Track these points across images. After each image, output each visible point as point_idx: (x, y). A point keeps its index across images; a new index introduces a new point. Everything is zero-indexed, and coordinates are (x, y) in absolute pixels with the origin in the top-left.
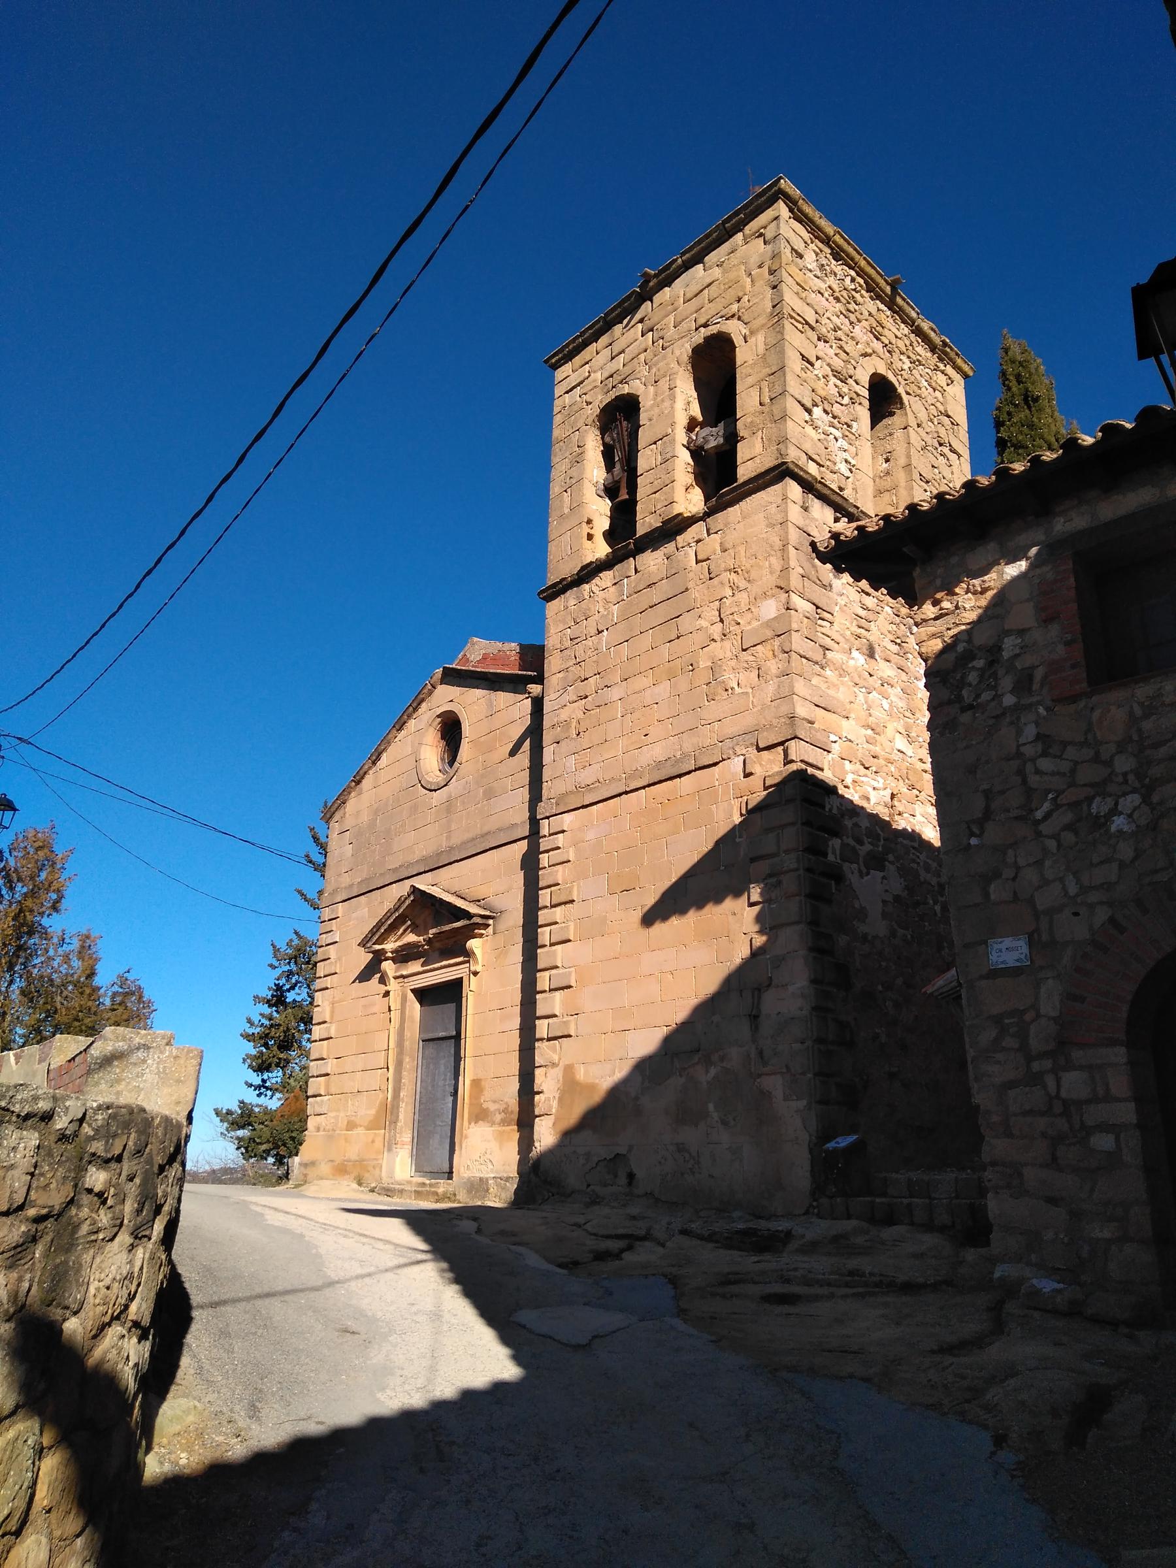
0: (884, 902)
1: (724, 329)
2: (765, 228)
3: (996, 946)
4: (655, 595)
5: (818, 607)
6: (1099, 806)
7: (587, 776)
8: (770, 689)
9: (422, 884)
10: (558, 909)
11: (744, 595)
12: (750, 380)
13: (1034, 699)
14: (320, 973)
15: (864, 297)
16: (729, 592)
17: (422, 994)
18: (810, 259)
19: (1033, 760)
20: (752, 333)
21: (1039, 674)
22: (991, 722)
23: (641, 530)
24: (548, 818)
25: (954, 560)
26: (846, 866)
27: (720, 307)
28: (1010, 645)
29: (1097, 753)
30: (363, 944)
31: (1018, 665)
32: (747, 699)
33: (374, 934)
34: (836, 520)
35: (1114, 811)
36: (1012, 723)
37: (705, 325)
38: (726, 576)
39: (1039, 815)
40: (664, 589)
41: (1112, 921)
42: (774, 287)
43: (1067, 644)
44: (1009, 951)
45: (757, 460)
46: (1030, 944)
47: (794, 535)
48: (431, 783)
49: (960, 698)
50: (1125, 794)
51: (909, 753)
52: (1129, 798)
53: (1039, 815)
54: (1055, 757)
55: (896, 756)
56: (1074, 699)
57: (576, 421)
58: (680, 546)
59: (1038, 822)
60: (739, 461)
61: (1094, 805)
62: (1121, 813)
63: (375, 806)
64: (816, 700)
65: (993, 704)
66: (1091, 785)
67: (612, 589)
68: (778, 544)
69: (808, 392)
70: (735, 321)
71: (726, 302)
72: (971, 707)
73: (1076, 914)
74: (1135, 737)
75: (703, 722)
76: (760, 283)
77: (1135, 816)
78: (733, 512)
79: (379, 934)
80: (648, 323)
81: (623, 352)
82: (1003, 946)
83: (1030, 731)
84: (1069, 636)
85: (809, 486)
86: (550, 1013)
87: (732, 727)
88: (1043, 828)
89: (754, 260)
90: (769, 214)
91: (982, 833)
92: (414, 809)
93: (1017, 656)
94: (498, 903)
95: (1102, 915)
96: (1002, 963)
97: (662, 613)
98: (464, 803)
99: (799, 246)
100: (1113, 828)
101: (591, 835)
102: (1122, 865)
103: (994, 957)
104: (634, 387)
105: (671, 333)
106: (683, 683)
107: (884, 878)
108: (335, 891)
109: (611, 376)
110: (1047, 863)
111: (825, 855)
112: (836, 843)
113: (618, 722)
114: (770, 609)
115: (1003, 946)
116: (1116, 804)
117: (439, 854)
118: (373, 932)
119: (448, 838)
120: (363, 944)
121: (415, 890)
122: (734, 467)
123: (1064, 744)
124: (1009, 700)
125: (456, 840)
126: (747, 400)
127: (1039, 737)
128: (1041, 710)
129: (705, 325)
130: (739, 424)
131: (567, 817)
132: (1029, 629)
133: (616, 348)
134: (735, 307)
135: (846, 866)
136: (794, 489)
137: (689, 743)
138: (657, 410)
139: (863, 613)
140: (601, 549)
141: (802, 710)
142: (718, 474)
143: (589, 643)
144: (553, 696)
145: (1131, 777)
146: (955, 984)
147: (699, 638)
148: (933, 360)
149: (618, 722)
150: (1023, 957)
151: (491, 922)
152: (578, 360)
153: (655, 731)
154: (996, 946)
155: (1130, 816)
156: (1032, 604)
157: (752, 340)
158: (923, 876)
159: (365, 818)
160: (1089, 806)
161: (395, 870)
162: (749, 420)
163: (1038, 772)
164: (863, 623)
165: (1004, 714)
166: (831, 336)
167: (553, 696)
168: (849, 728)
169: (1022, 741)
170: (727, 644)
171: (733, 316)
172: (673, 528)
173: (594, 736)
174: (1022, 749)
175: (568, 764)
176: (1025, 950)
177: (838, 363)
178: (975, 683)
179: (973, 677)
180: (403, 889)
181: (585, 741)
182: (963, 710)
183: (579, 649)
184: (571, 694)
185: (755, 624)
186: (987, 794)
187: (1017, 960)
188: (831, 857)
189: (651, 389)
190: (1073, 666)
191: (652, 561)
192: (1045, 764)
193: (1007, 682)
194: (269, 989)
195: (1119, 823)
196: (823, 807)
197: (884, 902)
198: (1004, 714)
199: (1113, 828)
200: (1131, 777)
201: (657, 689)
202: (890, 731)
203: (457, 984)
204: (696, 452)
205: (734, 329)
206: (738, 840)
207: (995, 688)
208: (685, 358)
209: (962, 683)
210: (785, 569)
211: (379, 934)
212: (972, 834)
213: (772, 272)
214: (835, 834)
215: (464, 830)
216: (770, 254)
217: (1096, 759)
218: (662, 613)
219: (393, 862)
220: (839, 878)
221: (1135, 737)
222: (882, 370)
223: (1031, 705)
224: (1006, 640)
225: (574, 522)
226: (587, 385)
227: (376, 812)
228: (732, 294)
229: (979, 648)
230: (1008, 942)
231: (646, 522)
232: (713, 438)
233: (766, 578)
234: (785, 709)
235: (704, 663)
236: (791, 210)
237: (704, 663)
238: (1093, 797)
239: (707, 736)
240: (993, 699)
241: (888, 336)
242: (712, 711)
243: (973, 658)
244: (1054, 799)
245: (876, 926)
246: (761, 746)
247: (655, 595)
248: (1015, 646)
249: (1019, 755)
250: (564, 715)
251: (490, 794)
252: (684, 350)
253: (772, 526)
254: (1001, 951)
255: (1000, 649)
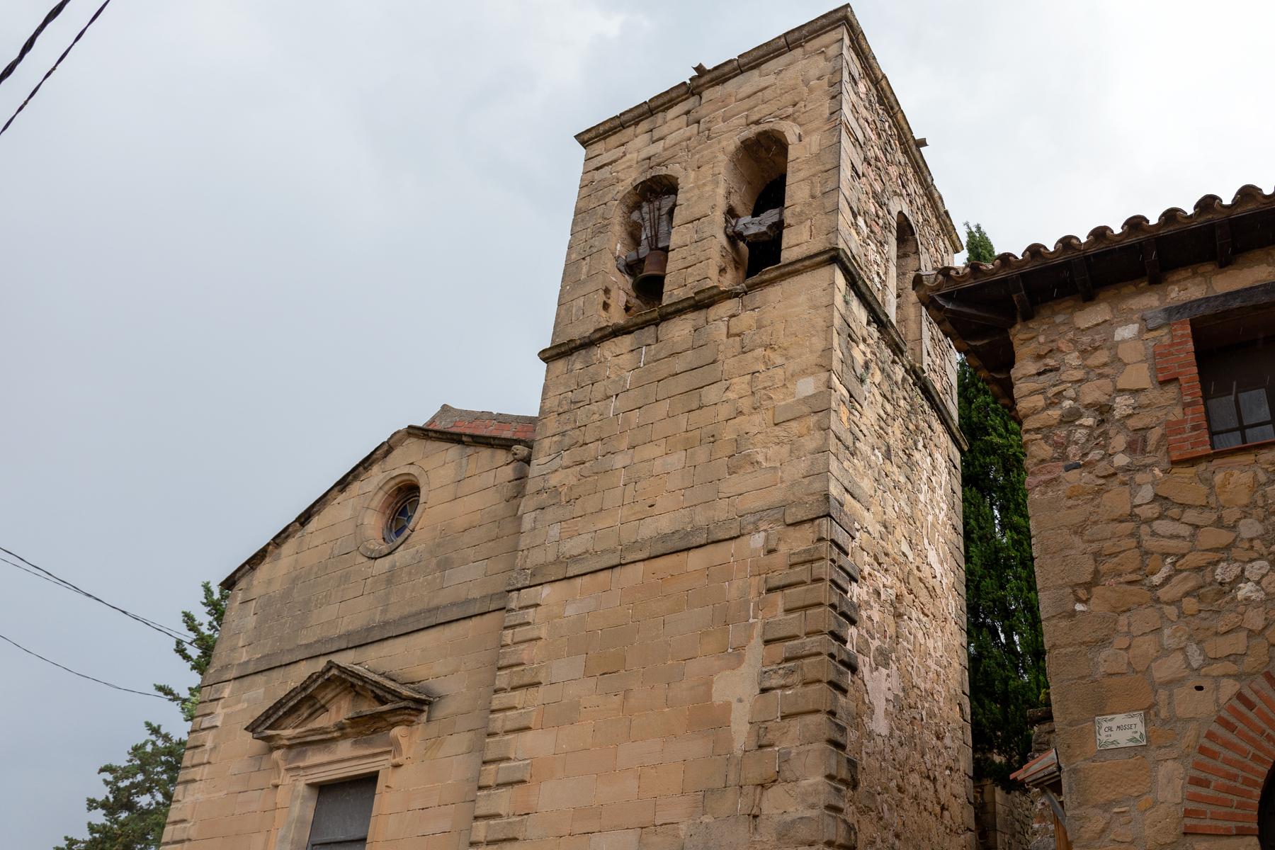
0: (887, 700)
1: (777, 127)
2: (827, 47)
3: (1105, 725)
4: (679, 364)
5: (851, 396)
6: (1224, 572)
7: (573, 546)
8: (803, 466)
9: (344, 660)
10: (517, 693)
11: (780, 371)
12: (802, 175)
13: (1149, 461)
14: (186, 762)
15: (895, 143)
16: (762, 367)
17: (324, 790)
18: (862, 88)
19: (1149, 521)
20: (807, 133)
21: (1154, 436)
22: (1102, 481)
23: (666, 300)
24: (519, 590)
25: (1059, 319)
26: (860, 657)
27: (775, 108)
28: (1122, 405)
29: (1220, 518)
30: (252, 728)
31: (1132, 423)
32: (775, 471)
33: (292, 698)
34: (869, 323)
35: (1241, 578)
36: (1124, 483)
37: (757, 123)
38: (759, 352)
39: (1156, 579)
40: (688, 359)
41: (1240, 696)
42: (834, 97)
43: (1186, 405)
44: (1120, 730)
45: (805, 247)
46: (1146, 722)
47: (837, 321)
48: (373, 551)
49: (1064, 457)
50: (1251, 560)
51: (911, 559)
52: (1257, 564)
53: (1156, 579)
54: (1173, 519)
55: (902, 559)
56: (1192, 461)
57: (603, 196)
58: (710, 319)
59: (1154, 588)
60: (784, 245)
61: (1219, 571)
62: (1248, 580)
63: (293, 575)
64: (846, 483)
65: (1104, 463)
66: (1216, 550)
67: (626, 357)
68: (820, 323)
69: (855, 199)
70: (789, 122)
71: (780, 104)
72: (1077, 466)
73: (1199, 688)
74: (1260, 503)
75: (721, 495)
76: (817, 93)
77: (1264, 582)
78: (774, 292)
79: (275, 717)
80: (693, 116)
81: (662, 139)
82: (1114, 724)
83: (1146, 493)
84: (1188, 399)
85: (854, 282)
86: (492, 812)
87: (753, 502)
88: (1160, 592)
89: (814, 72)
90: (833, 35)
91: (1088, 600)
92: (346, 578)
93: (1129, 416)
94: (438, 686)
95: (1229, 688)
96: (1112, 743)
97: (683, 383)
98: (410, 573)
99: (857, 76)
100: (1240, 595)
101: (570, 611)
102: (1251, 634)
103: (1103, 736)
104: (673, 169)
105: (719, 126)
106: (701, 454)
107: (888, 675)
108: (225, 667)
109: (649, 158)
110: (1167, 632)
111: (845, 642)
112: (852, 631)
113: (618, 491)
114: (807, 387)
115: (1114, 724)
116: (1243, 571)
117: (369, 630)
118: (267, 715)
119: (384, 612)
120: (252, 728)
121: (331, 666)
122: (780, 250)
123: (1184, 507)
124: (1121, 460)
125: (393, 615)
126: (797, 191)
127: (1157, 497)
128: (1157, 471)
129: (757, 123)
130: (787, 213)
131: (546, 591)
132: (1143, 390)
133: (656, 134)
134: (790, 110)
135: (860, 657)
136: (840, 280)
137: (701, 518)
138: (696, 192)
139: (885, 416)
140: (617, 317)
141: (835, 490)
142: (759, 257)
143: (594, 407)
144: (543, 460)
145: (1257, 544)
146: (1053, 768)
147: (724, 411)
148: (937, 227)
149: (618, 491)
150: (1137, 736)
151: (426, 708)
152: (613, 140)
153: (661, 503)
154: (1105, 725)
155: (1258, 583)
156: (1146, 365)
157: (806, 140)
158: (916, 680)
159: (277, 588)
160: (1214, 571)
161: (307, 646)
162: (798, 209)
163: (1154, 534)
164: (882, 424)
165: (1115, 474)
166: (873, 162)
167: (543, 460)
168: (869, 520)
169: (1137, 501)
170: (757, 418)
171: (788, 117)
172: (703, 302)
173: (591, 504)
174: (1137, 510)
175: (551, 533)
176: (1141, 729)
177: (878, 188)
178: (1083, 440)
179: (1080, 434)
180: (321, 664)
181: (577, 509)
182: (1068, 469)
183: (581, 415)
184: (567, 458)
185: (790, 400)
186: (1097, 556)
187: (1130, 740)
188: (849, 646)
189: (692, 175)
190: (1194, 428)
191: (679, 330)
192: (1163, 526)
193: (1119, 441)
194: (92, 805)
195: (1245, 590)
196: (846, 592)
197: (887, 700)
198: (1115, 474)
199: (1240, 595)
200: (1257, 544)
201: (669, 459)
202: (898, 533)
203: (370, 780)
204: (734, 238)
205: (790, 131)
206: (751, 621)
207: (1104, 447)
208: (732, 148)
209: (1068, 441)
210: (829, 349)
211: (275, 717)
212: (1079, 600)
213: (832, 85)
214: (853, 622)
215: (414, 595)
216: (830, 70)
217: (1219, 523)
218: (683, 383)
219: (307, 637)
220: (853, 669)
221: (1260, 503)
222: (906, 212)
223: (1145, 466)
224: (1118, 400)
225: (591, 287)
226: (620, 166)
227: (294, 581)
228: (788, 98)
229: (1087, 406)
230: (1120, 719)
231: (673, 292)
232: (753, 226)
233: (810, 358)
234: (817, 486)
235: (729, 434)
236: (851, 40)
237: (729, 434)
238: (1218, 562)
239: (721, 511)
240: (1102, 459)
241: (911, 189)
242: (732, 484)
243: (1081, 416)
244: (1174, 564)
245: (880, 725)
246: (789, 521)
247: (679, 364)
248: (1128, 406)
249: (1132, 516)
250: (554, 480)
251: (445, 565)
252: (731, 142)
253: (816, 308)
254: (1110, 729)
255: (1111, 409)
